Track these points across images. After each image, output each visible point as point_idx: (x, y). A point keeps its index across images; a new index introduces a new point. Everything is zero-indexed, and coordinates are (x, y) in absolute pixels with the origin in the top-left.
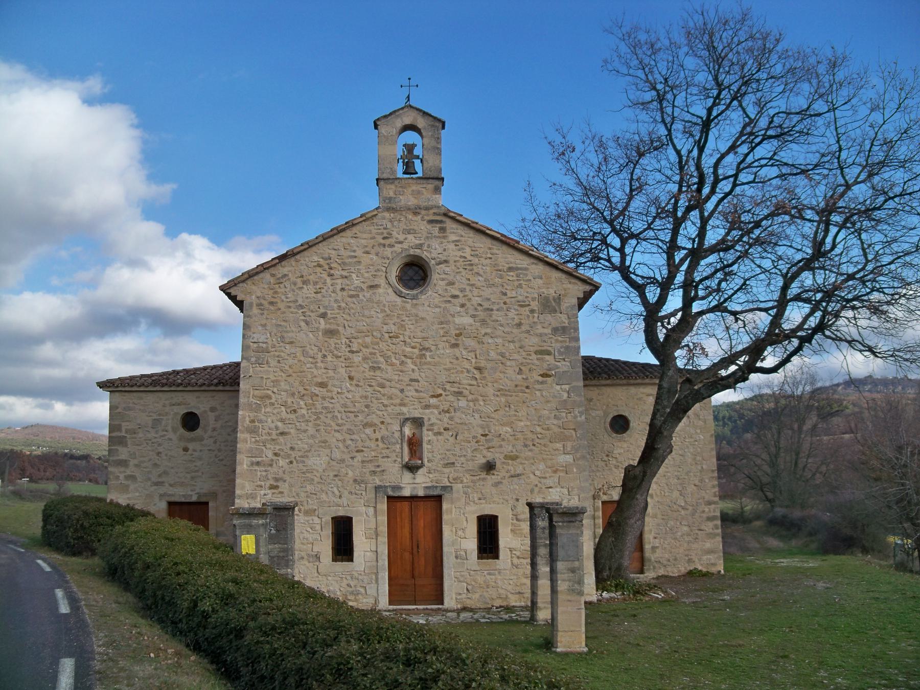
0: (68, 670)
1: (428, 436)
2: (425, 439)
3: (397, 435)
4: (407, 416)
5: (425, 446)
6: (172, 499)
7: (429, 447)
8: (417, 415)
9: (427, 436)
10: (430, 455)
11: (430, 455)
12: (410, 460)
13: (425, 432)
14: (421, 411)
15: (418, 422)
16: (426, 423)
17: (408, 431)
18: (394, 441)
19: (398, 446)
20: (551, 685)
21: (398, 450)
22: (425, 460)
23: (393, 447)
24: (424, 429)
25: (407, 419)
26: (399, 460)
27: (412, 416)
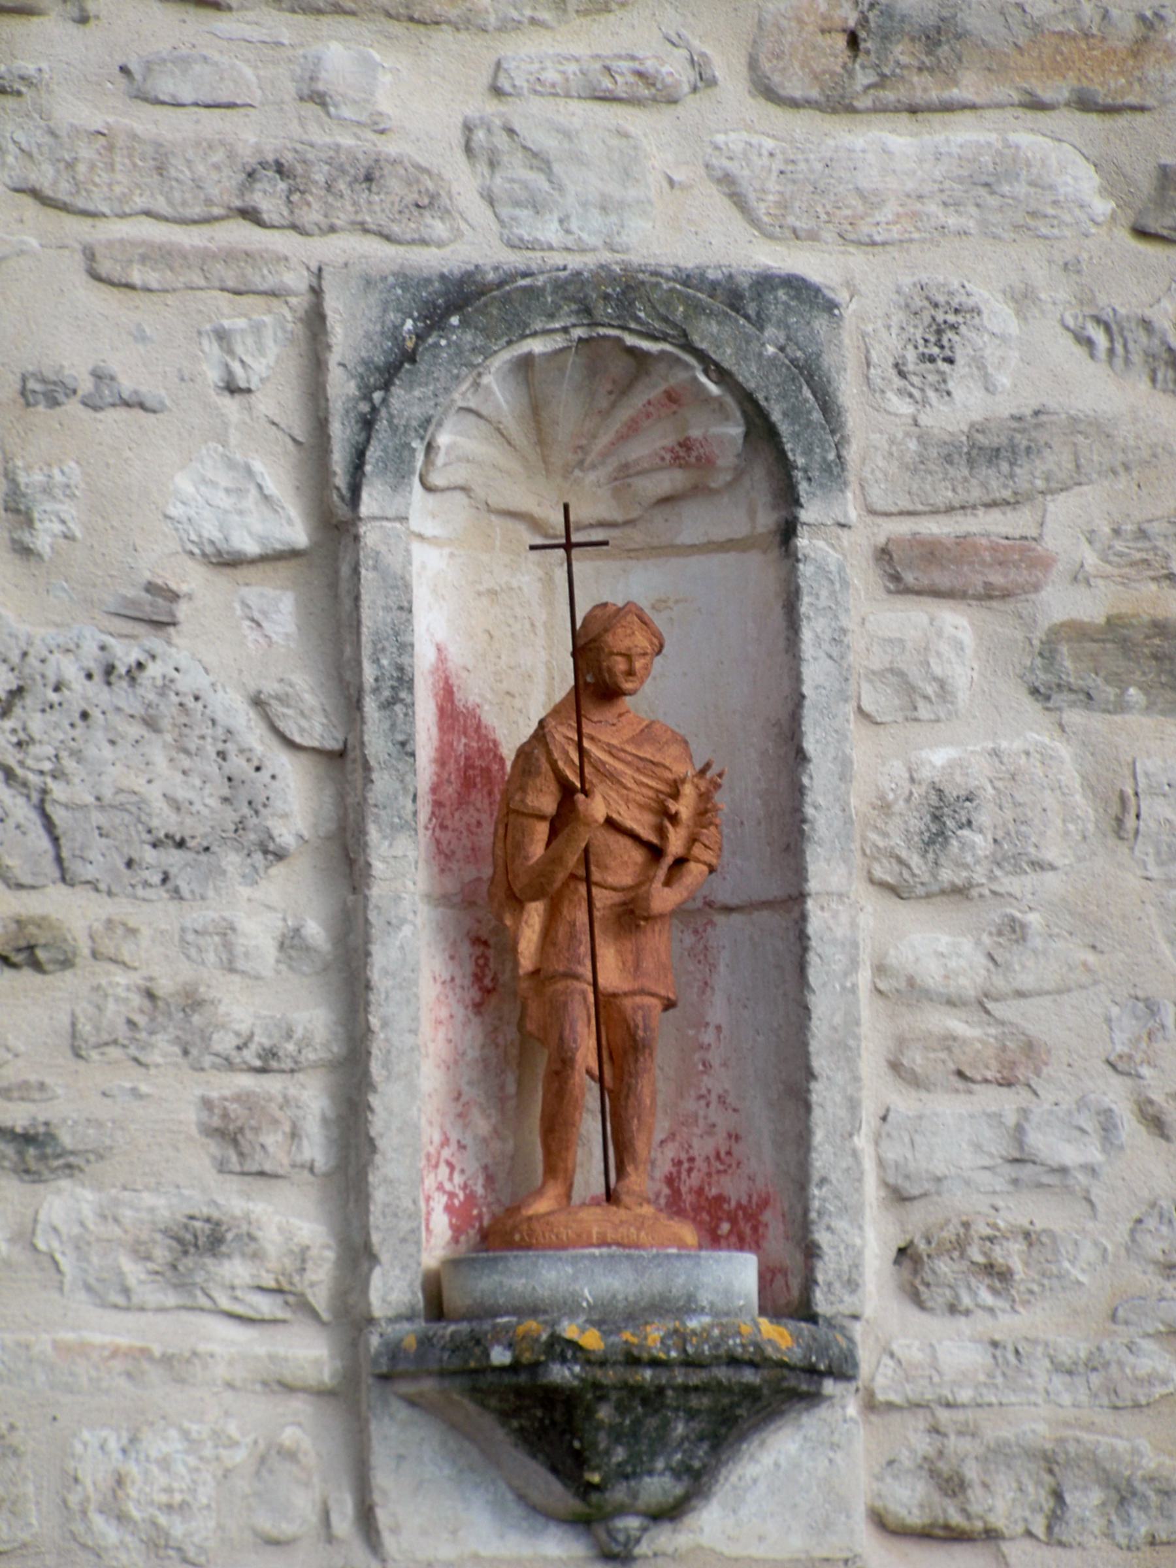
0: (289, 767)
1: (917, 696)
2: (858, 773)
3: (243, 651)
4: (469, 242)
5: (847, 917)
6: (615, 816)
7: (937, 947)
8: (676, 231)
9: (910, 704)
10: (954, 1135)
11: (954, 1135)
12: (496, 1232)
13: (855, 624)
14: (744, 130)
15: (695, 398)
16: (877, 421)
17: (470, 607)
18: (162, 782)
19: (270, 908)
20: (430, 1564)
21: (284, 1006)
22: (859, 1244)
23: (155, 939)
24: (838, 538)
25: (459, 305)
26: (290, 1223)
27: (568, 238)
